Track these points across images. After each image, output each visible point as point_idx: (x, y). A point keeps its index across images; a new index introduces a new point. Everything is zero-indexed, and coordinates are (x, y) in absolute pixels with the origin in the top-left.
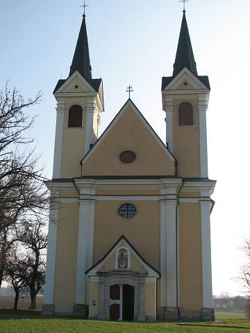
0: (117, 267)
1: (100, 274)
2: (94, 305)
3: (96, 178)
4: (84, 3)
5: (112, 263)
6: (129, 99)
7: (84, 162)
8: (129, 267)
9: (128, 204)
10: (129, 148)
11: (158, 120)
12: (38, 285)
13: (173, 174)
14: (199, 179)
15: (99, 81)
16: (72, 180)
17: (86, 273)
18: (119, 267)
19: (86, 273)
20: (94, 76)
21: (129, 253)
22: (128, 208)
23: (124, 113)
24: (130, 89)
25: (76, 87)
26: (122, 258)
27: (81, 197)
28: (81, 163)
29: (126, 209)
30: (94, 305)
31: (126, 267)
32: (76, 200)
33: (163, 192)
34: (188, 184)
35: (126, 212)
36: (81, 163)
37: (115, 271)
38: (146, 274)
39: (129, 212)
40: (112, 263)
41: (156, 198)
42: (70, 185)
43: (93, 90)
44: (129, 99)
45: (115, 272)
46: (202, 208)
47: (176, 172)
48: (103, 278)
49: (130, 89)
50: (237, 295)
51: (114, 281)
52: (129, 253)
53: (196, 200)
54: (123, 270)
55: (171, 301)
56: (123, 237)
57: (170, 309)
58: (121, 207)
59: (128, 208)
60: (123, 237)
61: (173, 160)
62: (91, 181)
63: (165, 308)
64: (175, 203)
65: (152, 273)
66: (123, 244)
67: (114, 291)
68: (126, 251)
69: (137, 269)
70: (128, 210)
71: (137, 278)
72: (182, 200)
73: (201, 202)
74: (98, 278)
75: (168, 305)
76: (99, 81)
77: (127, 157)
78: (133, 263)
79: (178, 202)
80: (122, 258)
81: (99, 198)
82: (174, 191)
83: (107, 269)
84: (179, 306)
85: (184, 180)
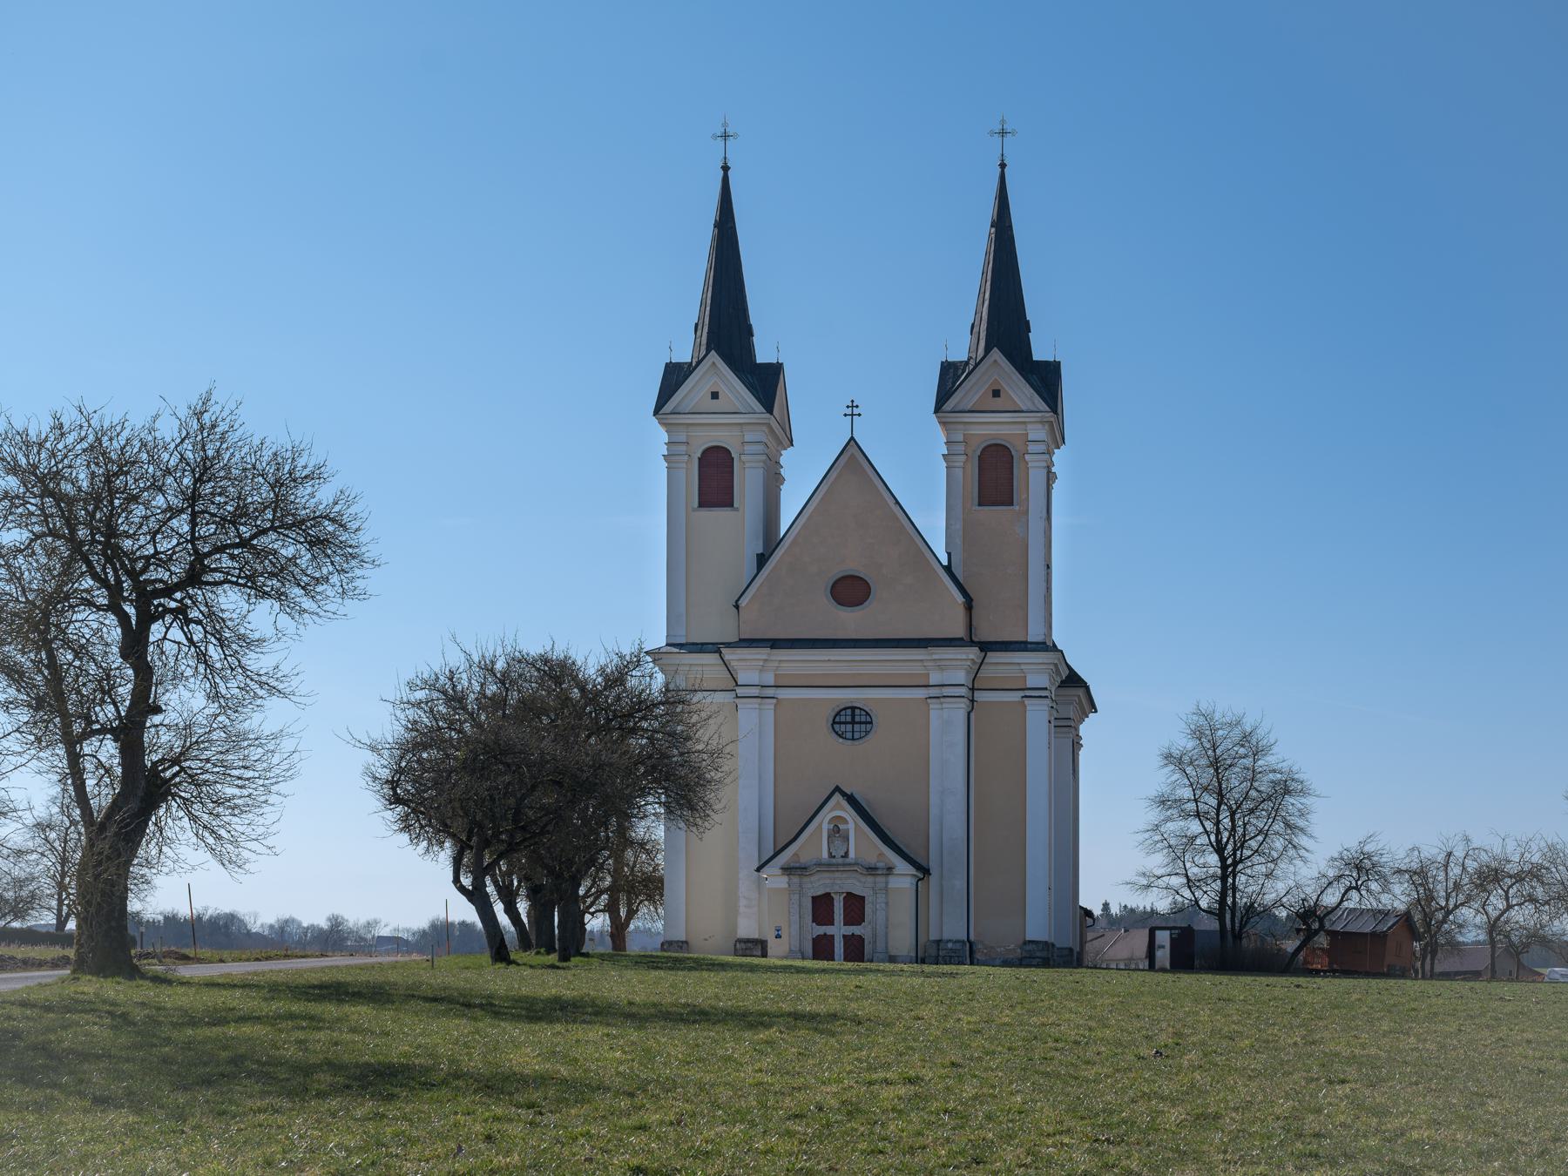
0: (825, 855)
1: (788, 870)
2: (778, 936)
3: (775, 644)
4: (725, 125)
5: (815, 845)
6: (852, 438)
7: (743, 603)
8: (852, 854)
9: (853, 709)
10: (853, 564)
11: (922, 484)
12: (629, 904)
13: (959, 631)
14: (1023, 646)
15: (775, 370)
16: (715, 648)
17: (758, 870)
18: (831, 856)
19: (758, 870)
20: (763, 355)
21: (851, 826)
22: (853, 716)
23: (804, 526)
24: (852, 411)
25: (715, 395)
26: (837, 832)
27: (740, 691)
28: (737, 607)
29: (849, 719)
30: (778, 936)
31: (846, 855)
32: (729, 696)
33: (935, 678)
34: (993, 657)
35: (849, 727)
36: (737, 607)
37: (820, 865)
38: (890, 870)
39: (857, 727)
40: (815, 845)
41: (920, 693)
42: (710, 659)
43: (758, 407)
44: (852, 438)
45: (827, 867)
46: (1028, 714)
47: (970, 627)
48: (796, 879)
49: (852, 411)
50: (226, 908)
51: (818, 885)
52: (851, 826)
53: (1015, 697)
54: (841, 861)
55: (954, 930)
56: (837, 789)
57: (950, 945)
58: (838, 714)
59: (853, 716)
60: (837, 789)
61: (960, 599)
62: (762, 654)
63: (938, 942)
64: (963, 705)
65: (902, 866)
66: (838, 806)
67: (821, 908)
68: (845, 821)
69: (871, 859)
70: (853, 722)
71: (870, 879)
72: (979, 696)
73: (1027, 701)
74: (785, 879)
75: (946, 937)
76: (775, 370)
77: (850, 591)
78: (861, 843)
79: (972, 701)
80: (837, 832)
81: (784, 694)
82: (961, 676)
83: (805, 859)
84: (972, 938)
85: (986, 647)
